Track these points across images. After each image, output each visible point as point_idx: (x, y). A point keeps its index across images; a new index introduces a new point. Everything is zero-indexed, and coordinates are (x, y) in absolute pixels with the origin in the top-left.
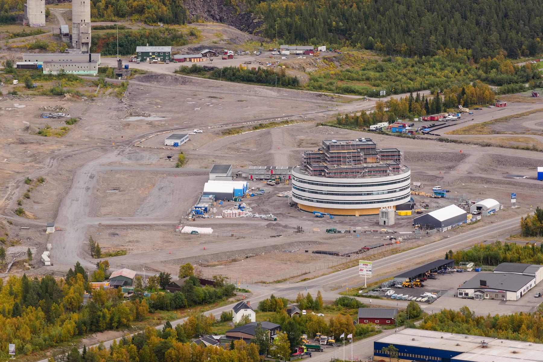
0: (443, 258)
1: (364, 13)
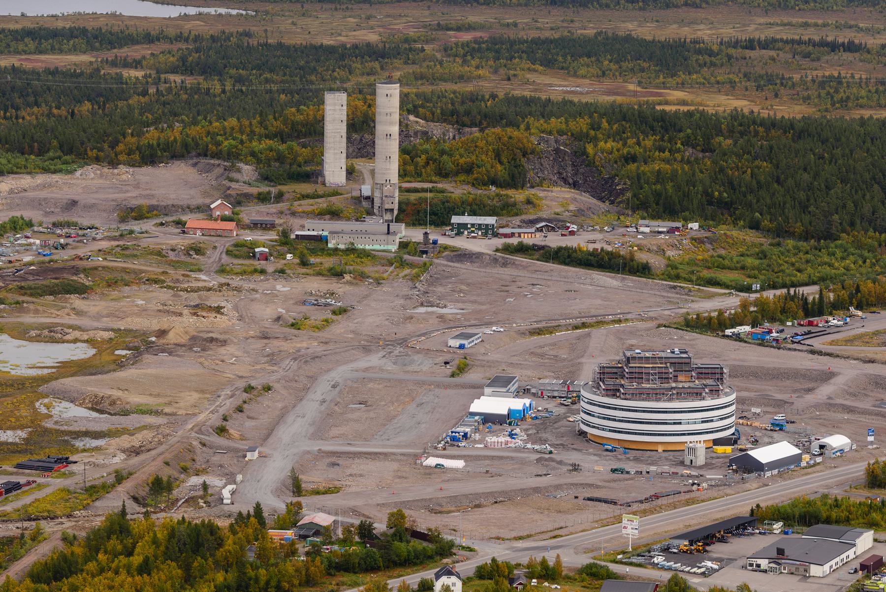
0: (748, 515)
1: (758, 183)
